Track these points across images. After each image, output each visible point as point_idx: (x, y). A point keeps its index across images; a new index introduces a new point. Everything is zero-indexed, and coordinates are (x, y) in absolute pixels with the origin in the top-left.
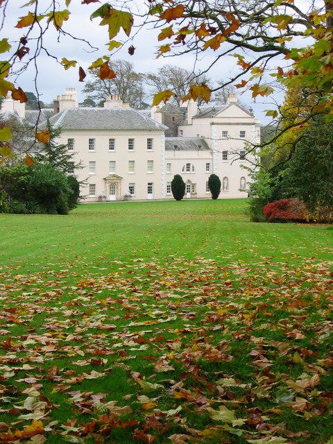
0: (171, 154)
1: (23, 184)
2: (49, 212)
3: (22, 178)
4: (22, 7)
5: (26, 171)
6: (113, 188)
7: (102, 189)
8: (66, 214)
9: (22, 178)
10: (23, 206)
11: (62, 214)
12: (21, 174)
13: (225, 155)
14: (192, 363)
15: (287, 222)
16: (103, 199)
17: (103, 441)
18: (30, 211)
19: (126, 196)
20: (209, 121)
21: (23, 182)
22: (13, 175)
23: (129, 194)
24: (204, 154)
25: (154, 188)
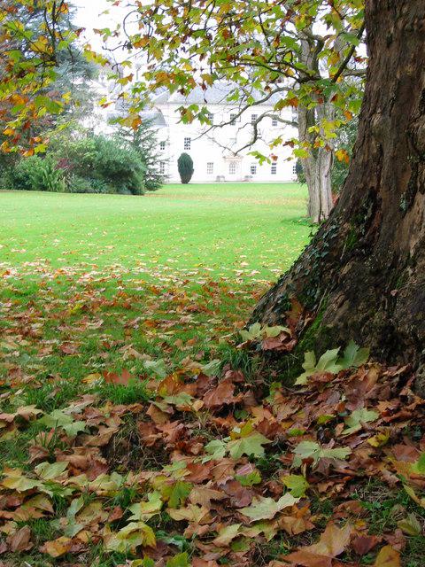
1: (89, 161)
2: (118, 192)
3: (88, 154)
4: (317, 362)
5: (93, 147)
7: (222, 169)
8: (143, 195)
9: (88, 154)
10: (87, 184)
11: (138, 194)
12: (88, 150)
14: (151, 147)
15: (29, 188)
16: (221, 179)
17: (244, 334)
18: (96, 189)
19: (247, 177)
21: (89, 158)
22: (79, 150)
23: (250, 174)
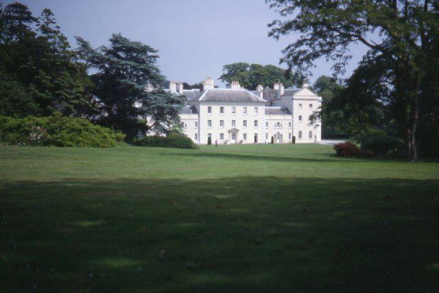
0: (268, 117)
6: (234, 135)
13: (300, 118)
20: (289, 98)
24: (288, 117)
25: (248, 137)
